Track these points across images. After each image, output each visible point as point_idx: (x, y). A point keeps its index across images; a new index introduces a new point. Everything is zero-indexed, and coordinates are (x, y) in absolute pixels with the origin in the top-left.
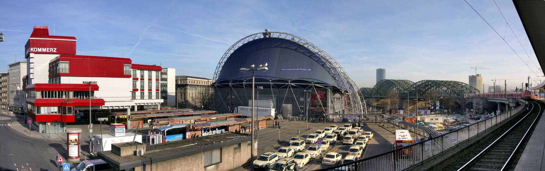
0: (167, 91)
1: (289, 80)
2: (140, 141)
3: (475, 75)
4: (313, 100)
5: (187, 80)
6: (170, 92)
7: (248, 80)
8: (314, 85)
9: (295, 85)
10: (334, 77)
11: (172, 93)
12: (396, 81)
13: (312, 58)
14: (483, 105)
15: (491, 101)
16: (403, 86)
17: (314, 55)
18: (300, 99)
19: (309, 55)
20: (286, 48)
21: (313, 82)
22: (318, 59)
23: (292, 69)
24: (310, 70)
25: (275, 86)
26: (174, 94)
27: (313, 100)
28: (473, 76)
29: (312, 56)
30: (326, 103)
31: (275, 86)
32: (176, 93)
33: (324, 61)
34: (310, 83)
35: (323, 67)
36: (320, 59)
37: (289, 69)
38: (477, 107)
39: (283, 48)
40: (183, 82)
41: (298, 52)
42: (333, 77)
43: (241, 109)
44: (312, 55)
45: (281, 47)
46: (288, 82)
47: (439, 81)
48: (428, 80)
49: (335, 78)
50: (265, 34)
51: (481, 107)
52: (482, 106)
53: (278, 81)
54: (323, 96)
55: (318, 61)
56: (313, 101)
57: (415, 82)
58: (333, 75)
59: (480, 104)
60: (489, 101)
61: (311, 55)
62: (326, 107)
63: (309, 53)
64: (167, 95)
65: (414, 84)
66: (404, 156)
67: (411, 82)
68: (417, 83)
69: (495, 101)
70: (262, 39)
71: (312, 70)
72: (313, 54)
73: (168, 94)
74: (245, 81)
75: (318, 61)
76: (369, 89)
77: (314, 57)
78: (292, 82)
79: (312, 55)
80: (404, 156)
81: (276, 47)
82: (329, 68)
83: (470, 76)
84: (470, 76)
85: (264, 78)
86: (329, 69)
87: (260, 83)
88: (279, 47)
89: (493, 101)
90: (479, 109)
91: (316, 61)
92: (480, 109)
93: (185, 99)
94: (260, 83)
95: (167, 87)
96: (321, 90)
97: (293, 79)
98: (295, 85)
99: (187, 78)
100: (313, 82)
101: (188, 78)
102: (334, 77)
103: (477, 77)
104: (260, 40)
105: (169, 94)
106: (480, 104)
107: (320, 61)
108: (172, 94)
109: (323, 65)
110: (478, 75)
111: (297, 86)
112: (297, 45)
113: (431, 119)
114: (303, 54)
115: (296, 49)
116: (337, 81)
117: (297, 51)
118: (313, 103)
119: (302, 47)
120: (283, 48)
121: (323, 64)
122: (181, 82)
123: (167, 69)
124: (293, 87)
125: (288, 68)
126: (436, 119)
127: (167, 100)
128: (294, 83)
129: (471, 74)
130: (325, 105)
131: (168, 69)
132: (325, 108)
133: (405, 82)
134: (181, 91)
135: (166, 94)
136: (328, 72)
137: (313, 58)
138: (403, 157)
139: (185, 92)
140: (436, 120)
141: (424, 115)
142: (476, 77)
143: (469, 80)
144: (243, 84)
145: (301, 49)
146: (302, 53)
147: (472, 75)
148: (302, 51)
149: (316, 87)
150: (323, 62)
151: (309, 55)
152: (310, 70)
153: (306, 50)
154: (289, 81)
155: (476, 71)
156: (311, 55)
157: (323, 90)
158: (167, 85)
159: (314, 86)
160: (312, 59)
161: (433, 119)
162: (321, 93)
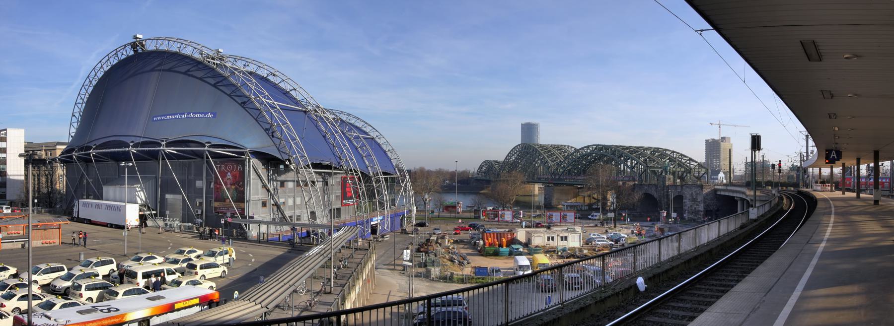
0: (6, 172)
1: (163, 141)
2: (810, 170)
3: (717, 138)
4: (218, 186)
5: (56, 149)
6: (11, 174)
7: (100, 145)
8: (208, 151)
9: (176, 152)
10: (271, 131)
11: (17, 175)
12: (544, 146)
13: (219, 87)
14: (705, 202)
15: (723, 193)
16: (557, 157)
17: (224, 82)
18: (195, 184)
19: (212, 81)
20: (170, 70)
21: (210, 143)
22: (233, 88)
23: (173, 117)
24: (210, 115)
25: (146, 156)
26: (23, 178)
27: (218, 186)
28: (713, 140)
29: (219, 84)
30: (243, 192)
31: (146, 156)
32: (26, 175)
33: (248, 94)
34: (203, 145)
35: (244, 108)
36: (237, 89)
37: (168, 117)
38: (691, 206)
39: (164, 70)
40: (51, 155)
41: (190, 78)
42: (266, 130)
43: (85, 205)
44: (221, 81)
45: (160, 70)
46: (160, 145)
47: (621, 146)
48: (598, 145)
49: (273, 133)
50: (134, 45)
51: (701, 207)
52: (702, 205)
53: (144, 144)
54: (238, 175)
55: (234, 94)
56: (218, 188)
57: (578, 148)
58: (268, 126)
59: (699, 200)
60: (719, 193)
61: (218, 82)
62: (244, 202)
63: (213, 77)
64: (6, 179)
65: (577, 151)
66: (577, 286)
67: (572, 147)
68: (583, 148)
69: (731, 194)
70: (132, 56)
71: (214, 117)
72: (221, 79)
73: (8, 177)
74: (94, 147)
75: (234, 94)
76: (497, 162)
77: (224, 86)
78: (170, 144)
79: (221, 81)
80: (577, 286)
81: (153, 70)
82: (259, 110)
83: (707, 141)
84: (707, 141)
85: (121, 140)
86: (259, 112)
87: (113, 150)
88: (157, 71)
89: (727, 194)
90: (696, 212)
91: (229, 95)
92: (699, 211)
93: (52, 188)
94: (113, 150)
95: (6, 164)
96: (233, 161)
97: (172, 138)
98: (176, 152)
99: (56, 146)
100: (210, 143)
101: (58, 147)
102: (271, 131)
103: (722, 143)
104: (129, 59)
105: (11, 177)
106: (699, 200)
107: (238, 94)
108: (16, 178)
109: (243, 104)
110: (723, 139)
111: (178, 153)
112: (191, 62)
113: (549, 238)
114: (200, 81)
115: (188, 71)
116: (277, 141)
117: (189, 75)
118: (218, 192)
119: (200, 66)
120: (164, 70)
121: (245, 99)
122: (46, 154)
123: (6, 130)
124: (170, 156)
125: (166, 115)
126: (562, 238)
127: (6, 190)
128: (171, 147)
129: (709, 137)
130: (241, 198)
131: (8, 130)
132: (241, 205)
133: (559, 148)
134: (34, 172)
135: (4, 177)
136: (256, 119)
137: (221, 88)
138: (575, 288)
139: (27, 173)
140: (562, 240)
141: (561, 222)
142: (719, 144)
143: (705, 148)
144: (90, 153)
145: (199, 69)
146: (200, 79)
147: (713, 138)
148: (199, 74)
149: (215, 156)
150: (246, 96)
151: (212, 81)
152: (210, 115)
153: (210, 70)
154: (163, 143)
155: (720, 130)
156: (218, 82)
157: (238, 163)
158: (6, 160)
159: (210, 152)
160: (219, 92)
161: (553, 238)
162: (233, 169)
